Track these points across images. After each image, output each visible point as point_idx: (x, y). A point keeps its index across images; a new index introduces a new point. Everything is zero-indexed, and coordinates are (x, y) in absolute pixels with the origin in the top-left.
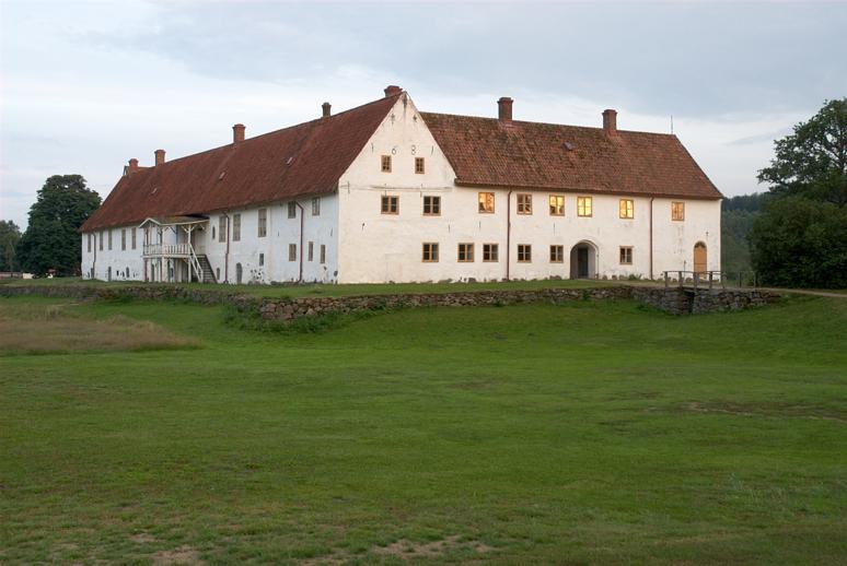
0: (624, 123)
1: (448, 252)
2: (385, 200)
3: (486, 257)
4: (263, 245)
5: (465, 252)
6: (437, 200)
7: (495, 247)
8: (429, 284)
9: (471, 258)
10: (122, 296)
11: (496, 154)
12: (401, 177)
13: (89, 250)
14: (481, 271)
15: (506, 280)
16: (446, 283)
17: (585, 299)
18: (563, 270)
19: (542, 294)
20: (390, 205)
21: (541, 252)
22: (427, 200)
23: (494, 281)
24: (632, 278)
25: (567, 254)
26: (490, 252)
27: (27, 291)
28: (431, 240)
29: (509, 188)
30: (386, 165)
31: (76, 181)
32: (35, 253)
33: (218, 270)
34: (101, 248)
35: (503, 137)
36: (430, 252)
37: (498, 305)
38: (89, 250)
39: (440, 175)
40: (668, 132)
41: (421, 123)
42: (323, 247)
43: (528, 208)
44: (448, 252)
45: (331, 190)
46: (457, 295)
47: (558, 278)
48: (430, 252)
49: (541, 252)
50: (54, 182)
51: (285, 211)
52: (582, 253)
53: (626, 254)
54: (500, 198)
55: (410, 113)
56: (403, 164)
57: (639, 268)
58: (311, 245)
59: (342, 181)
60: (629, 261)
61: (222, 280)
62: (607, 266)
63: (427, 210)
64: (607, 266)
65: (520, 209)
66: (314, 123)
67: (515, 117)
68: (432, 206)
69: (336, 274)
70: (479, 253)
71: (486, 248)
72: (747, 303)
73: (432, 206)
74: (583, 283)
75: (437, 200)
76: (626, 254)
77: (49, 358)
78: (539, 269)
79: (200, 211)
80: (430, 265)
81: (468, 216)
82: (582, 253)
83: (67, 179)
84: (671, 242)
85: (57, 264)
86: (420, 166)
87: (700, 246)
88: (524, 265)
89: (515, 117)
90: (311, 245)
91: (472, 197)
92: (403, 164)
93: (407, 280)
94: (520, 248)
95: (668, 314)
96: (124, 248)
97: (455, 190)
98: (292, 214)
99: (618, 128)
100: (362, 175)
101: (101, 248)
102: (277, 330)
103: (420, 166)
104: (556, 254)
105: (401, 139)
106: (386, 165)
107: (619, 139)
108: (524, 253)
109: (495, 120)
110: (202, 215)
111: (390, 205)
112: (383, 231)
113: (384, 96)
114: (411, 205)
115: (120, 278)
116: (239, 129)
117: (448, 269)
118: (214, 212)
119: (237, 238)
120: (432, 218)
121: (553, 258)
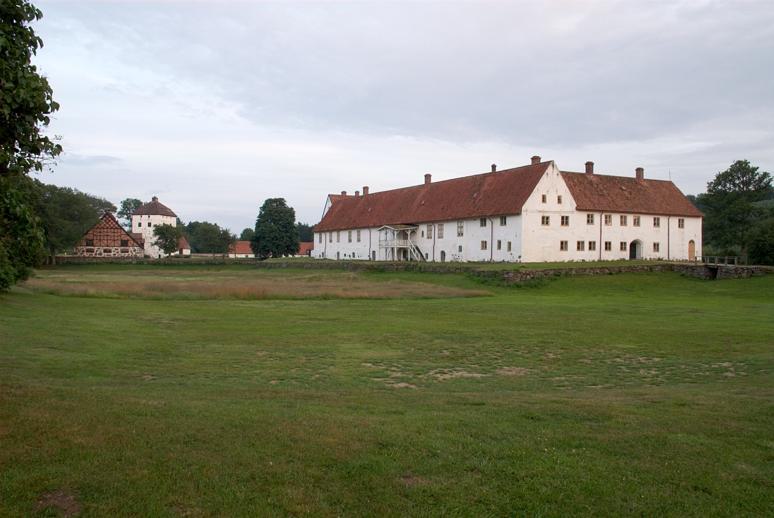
0: (647, 176)
1: (572, 246)
2: (543, 218)
3: (590, 248)
4: (460, 241)
5: (580, 245)
6: (567, 218)
7: (594, 243)
8: (563, 262)
9: (583, 249)
10: (326, 265)
11: (596, 193)
12: (552, 208)
13: (320, 241)
14: (588, 256)
15: (600, 261)
16: (571, 262)
17: (636, 272)
18: (626, 255)
19: (604, 269)
20: (545, 221)
21: (616, 246)
22: (563, 218)
23: (594, 261)
24: (659, 259)
25: (628, 247)
26: (592, 245)
27: (284, 266)
28: (564, 239)
29: (602, 211)
30: (544, 199)
31: (281, 202)
32: (263, 243)
33: (427, 255)
34: (331, 241)
35: (591, 183)
36: (564, 245)
37: (611, 274)
38: (320, 241)
39: (569, 204)
40: (668, 179)
41: (560, 177)
42: (510, 244)
43: (658, 224)
44: (572, 246)
45: (517, 213)
46: (592, 269)
47: (624, 260)
48: (564, 245)
49: (616, 246)
50: (269, 202)
51: (478, 223)
52: (634, 245)
53: (656, 246)
54: (597, 217)
55: (556, 172)
56: (552, 199)
57: (662, 254)
58: (499, 242)
59: (524, 208)
60: (658, 250)
61: (430, 259)
62: (647, 253)
63: (563, 223)
64: (647, 253)
65: (606, 222)
66: (485, 176)
67: (595, 172)
68: (565, 221)
69: (520, 257)
70: (587, 246)
71: (590, 243)
72: (713, 273)
73: (565, 221)
74: (633, 263)
75: (567, 218)
76: (656, 246)
77: (299, 302)
78: (616, 255)
79: (413, 221)
80: (564, 252)
81: (581, 228)
82: (634, 245)
83: (276, 201)
84: (679, 240)
85: (274, 249)
86: (559, 201)
87: (692, 242)
88: (608, 252)
89: (595, 172)
90: (499, 242)
91: (583, 216)
92: (552, 199)
93: (553, 261)
94: (606, 243)
95: (700, 279)
96: (350, 241)
97: (577, 213)
98: (483, 224)
99: (645, 177)
100: (532, 204)
101: (331, 241)
102: (518, 286)
103: (559, 201)
104: (623, 245)
105: (551, 185)
106: (544, 199)
107: (645, 184)
108: (608, 246)
109: (581, 174)
110: (415, 225)
111: (545, 221)
112: (542, 233)
113: (530, 163)
114: (555, 220)
115: (347, 258)
116: (428, 177)
117: (572, 255)
118: (423, 223)
119: (441, 237)
120: (565, 228)
121: (621, 249)
